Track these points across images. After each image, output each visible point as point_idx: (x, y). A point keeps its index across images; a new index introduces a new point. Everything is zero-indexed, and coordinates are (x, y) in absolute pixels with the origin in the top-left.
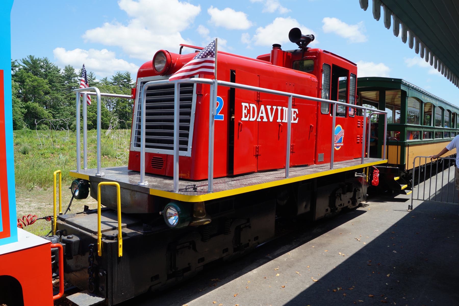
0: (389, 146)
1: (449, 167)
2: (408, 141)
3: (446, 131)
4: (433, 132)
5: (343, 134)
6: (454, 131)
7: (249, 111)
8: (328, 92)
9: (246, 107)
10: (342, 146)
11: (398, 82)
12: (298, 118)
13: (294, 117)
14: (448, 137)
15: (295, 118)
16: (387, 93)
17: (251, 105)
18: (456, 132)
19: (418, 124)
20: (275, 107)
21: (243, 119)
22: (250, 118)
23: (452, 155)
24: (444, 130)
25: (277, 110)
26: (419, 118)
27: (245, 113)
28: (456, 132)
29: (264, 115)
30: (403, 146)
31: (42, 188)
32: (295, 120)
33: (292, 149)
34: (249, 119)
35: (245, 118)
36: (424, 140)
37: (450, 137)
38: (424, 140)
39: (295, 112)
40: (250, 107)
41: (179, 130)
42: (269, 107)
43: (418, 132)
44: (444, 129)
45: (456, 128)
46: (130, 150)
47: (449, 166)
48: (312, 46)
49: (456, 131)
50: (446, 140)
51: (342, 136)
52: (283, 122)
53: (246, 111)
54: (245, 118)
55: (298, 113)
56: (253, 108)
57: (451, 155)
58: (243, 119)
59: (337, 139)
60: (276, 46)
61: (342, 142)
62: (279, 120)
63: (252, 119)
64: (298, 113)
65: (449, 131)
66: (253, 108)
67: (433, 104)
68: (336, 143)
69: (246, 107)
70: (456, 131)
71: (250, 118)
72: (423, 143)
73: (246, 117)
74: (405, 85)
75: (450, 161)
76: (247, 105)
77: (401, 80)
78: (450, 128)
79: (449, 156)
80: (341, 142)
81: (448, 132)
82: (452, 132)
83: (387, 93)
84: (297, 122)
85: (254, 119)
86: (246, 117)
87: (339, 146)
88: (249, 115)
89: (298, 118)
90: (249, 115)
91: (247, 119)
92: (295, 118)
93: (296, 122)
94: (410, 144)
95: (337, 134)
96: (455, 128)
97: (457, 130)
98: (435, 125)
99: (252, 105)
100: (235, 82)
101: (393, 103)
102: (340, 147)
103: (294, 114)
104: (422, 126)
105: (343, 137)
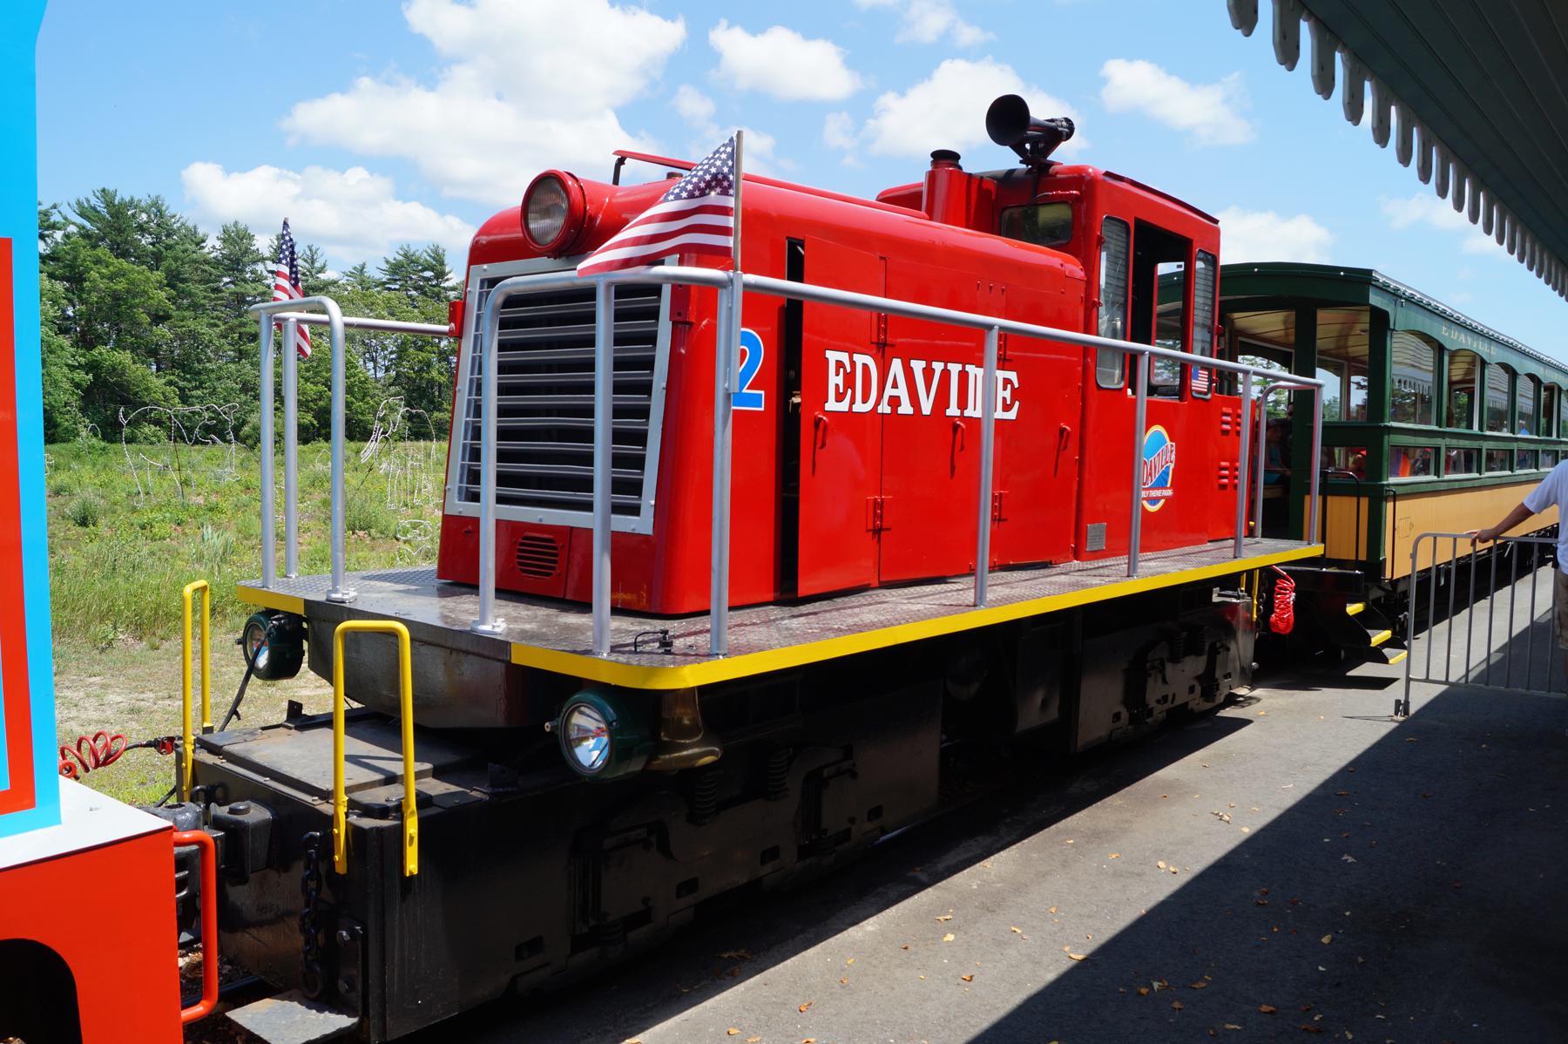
0: (1329, 498)
1: (1534, 568)
2: (1392, 480)
3: (1525, 446)
4: (1479, 451)
5: (1173, 457)
6: (1552, 447)
7: (849, 380)
8: (1120, 313)
9: (840, 364)
10: (1167, 498)
11: (1361, 280)
12: (1017, 403)
13: (1004, 399)
14: (1531, 468)
15: (1008, 402)
16: (1323, 316)
17: (856, 357)
18: (1557, 452)
19: (1429, 423)
20: (938, 366)
21: (832, 405)
22: (853, 401)
23: (1545, 528)
24: (1515, 444)
25: (946, 374)
26: (1430, 401)
27: (837, 386)
28: (1557, 452)
29: (902, 391)
30: (1378, 497)
31: (144, 643)
32: (1007, 408)
33: (997, 508)
34: (850, 407)
35: (837, 401)
36: (1447, 477)
37: (1537, 468)
38: (1447, 477)
39: (1007, 381)
40: (853, 364)
41: (613, 444)
42: (918, 366)
43: (1429, 450)
44: (1517, 440)
45: (1558, 436)
46: (445, 513)
47: (1535, 565)
48: (1064, 155)
49: (1557, 448)
50: (1524, 478)
51: (1167, 463)
52: (965, 415)
53: (840, 380)
54: (837, 401)
55: (1016, 386)
56: (866, 367)
57: (1541, 530)
58: (832, 405)
59: (1151, 475)
60: (944, 158)
61: (1169, 485)
62: (953, 411)
63: (860, 407)
64: (1016, 386)
65: (1532, 447)
66: (866, 367)
67: (1480, 356)
68: (1147, 486)
69: (840, 364)
70: (1557, 448)
71: (853, 401)
72: (1444, 486)
73: (840, 398)
74: (1384, 289)
75: (1536, 548)
76: (844, 357)
77: (1369, 272)
78: (1536, 437)
79: (1534, 532)
80: (1167, 483)
81: (1531, 451)
82: (1543, 451)
83: (1323, 316)
84: (1014, 418)
85: (868, 407)
86: (840, 398)
87: (1157, 499)
88: (850, 391)
89: (1017, 403)
90: (850, 391)
91: (843, 406)
92: (1008, 402)
93: (1012, 415)
94: (1400, 490)
95: (1153, 458)
96: (1554, 437)
97: (1561, 442)
98: (1485, 428)
99: (860, 359)
100: (802, 281)
101: (1343, 351)
102: (1162, 501)
103: (1005, 389)
104: (1441, 429)
105: (1172, 466)
